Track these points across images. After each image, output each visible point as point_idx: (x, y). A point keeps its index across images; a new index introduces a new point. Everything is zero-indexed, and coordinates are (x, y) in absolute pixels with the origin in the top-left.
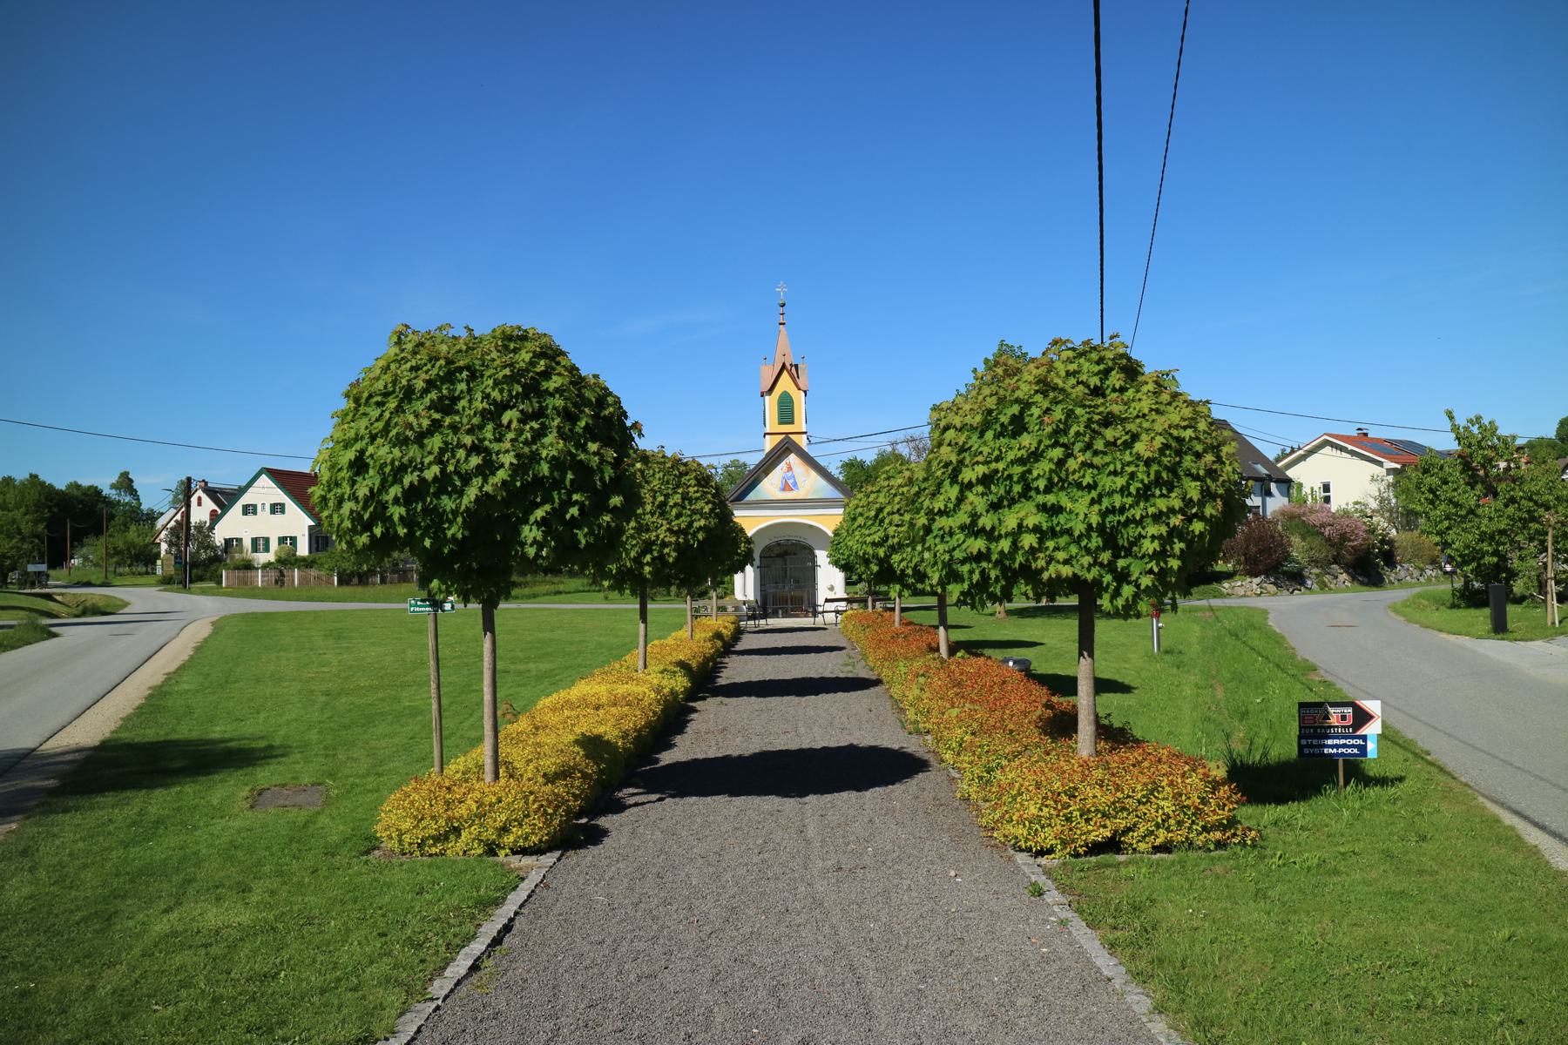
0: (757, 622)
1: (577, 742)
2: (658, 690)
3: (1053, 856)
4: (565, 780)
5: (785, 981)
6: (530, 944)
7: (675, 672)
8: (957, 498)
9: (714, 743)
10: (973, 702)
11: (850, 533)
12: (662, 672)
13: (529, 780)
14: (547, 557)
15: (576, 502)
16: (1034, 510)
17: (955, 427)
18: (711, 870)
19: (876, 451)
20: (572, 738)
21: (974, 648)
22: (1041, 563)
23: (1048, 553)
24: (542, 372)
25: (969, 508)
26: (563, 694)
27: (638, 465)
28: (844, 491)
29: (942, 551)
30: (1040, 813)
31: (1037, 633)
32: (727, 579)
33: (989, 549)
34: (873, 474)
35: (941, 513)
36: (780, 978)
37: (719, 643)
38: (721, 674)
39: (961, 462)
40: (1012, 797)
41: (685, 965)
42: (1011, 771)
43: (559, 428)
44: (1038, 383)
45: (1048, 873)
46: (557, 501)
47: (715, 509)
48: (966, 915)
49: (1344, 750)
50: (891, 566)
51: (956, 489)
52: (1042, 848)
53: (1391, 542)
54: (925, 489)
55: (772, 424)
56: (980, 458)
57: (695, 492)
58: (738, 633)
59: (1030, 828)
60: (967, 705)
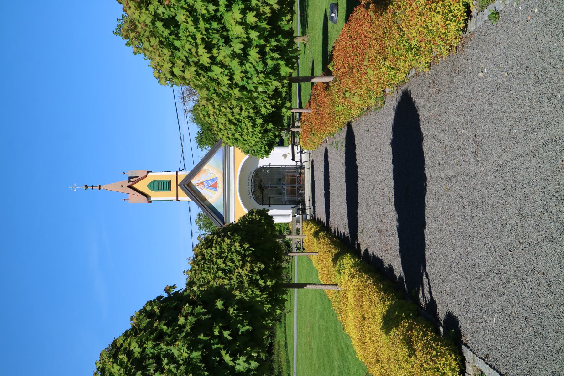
0: (307, 208)
1: (387, 333)
2: (352, 276)
3: (471, 4)
4: (413, 342)
5: (554, 191)
6: (527, 369)
7: (340, 264)
8: (221, 67)
9: (389, 238)
10: (363, 60)
11: (246, 142)
12: (340, 274)
13: (413, 367)
14: (258, 353)
15: (220, 332)
16: (230, 13)
17: (171, 68)
18: (475, 241)
19: (191, 124)
20: (384, 337)
21: (327, 58)
22: (267, 10)
23: (260, 5)
24: (127, 357)
25: (228, 59)
26: (354, 343)
27: (195, 288)
28: (218, 146)
29: (258, 79)
30: (441, 13)
31: (318, 15)
32: (277, 228)
33: (257, 46)
34: (207, 126)
35: (231, 79)
36: (551, 195)
37: (321, 234)
38: (342, 233)
39: (196, 64)
40: (429, 33)
41: (542, 260)
42: (411, 33)
43: (167, 345)
44: (141, 8)
45: (483, 8)
46: (218, 346)
47: (228, 236)
48: (510, 65)
50: (269, 115)
51: (214, 68)
52: (465, 12)
54: (214, 90)
55: (170, 195)
56: (194, 50)
57: (216, 249)
58: (315, 221)
59: (451, 20)
60: (365, 63)
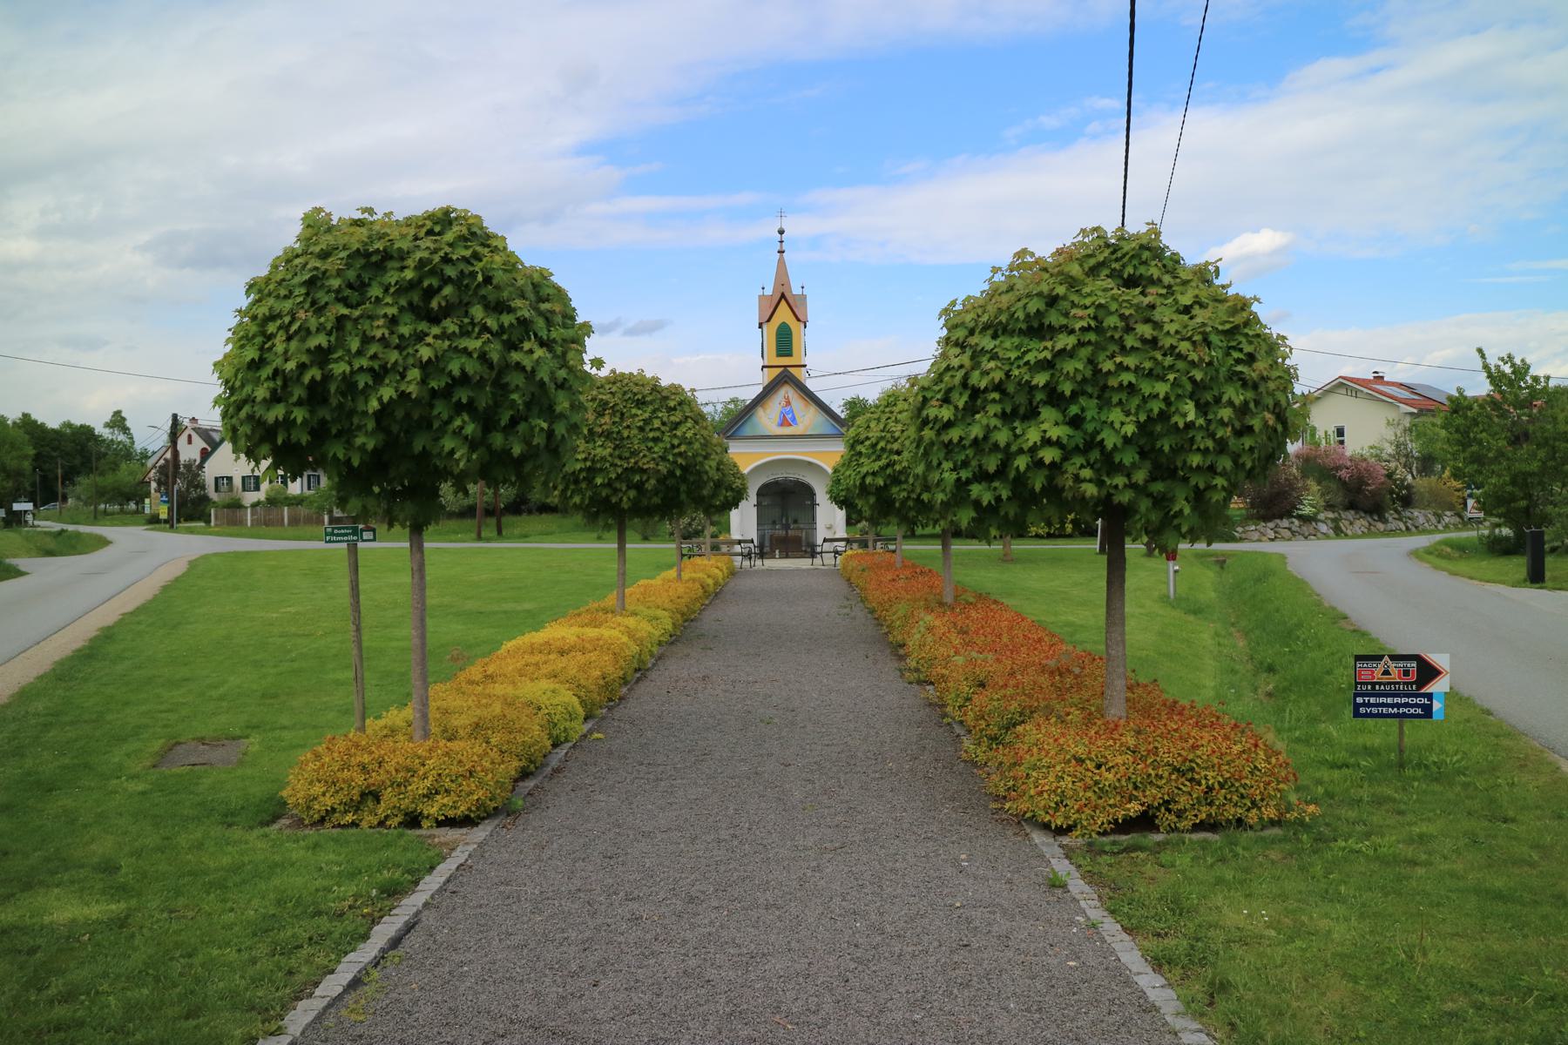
49: (1406, 710)
53: (1409, 487)
